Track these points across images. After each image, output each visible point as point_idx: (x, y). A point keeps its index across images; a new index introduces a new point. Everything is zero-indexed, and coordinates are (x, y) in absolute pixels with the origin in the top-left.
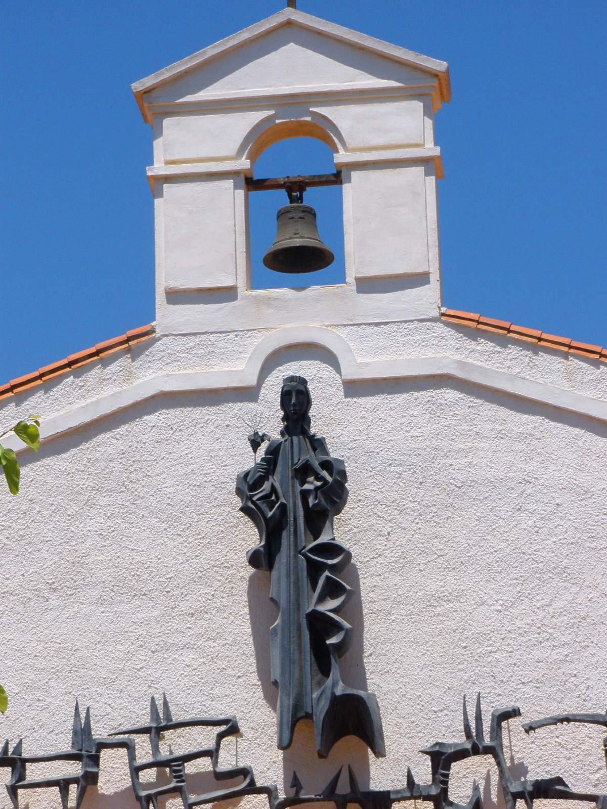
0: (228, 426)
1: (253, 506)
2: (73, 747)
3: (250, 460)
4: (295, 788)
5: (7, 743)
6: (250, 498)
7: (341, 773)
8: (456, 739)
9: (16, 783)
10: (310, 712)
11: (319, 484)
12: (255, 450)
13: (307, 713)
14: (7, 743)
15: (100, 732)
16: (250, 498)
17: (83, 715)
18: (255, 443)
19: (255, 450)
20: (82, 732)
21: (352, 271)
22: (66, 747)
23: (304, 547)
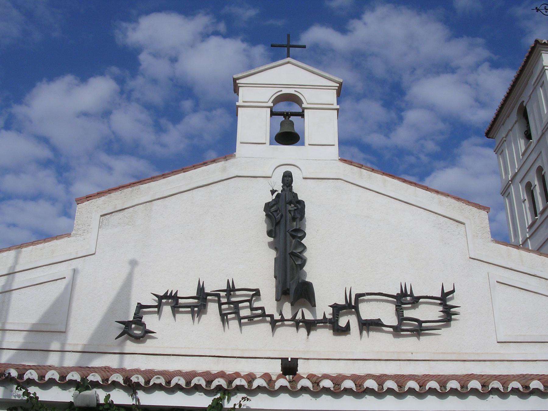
0: (260, 189)
1: (271, 214)
2: (197, 295)
3: (270, 198)
4: (281, 316)
5: (168, 291)
6: (270, 211)
7: (435, 336)
8: (342, 302)
9: (175, 305)
10: (289, 288)
11: (296, 208)
12: (272, 195)
13: (288, 288)
14: (168, 291)
15: (207, 290)
16: (270, 211)
17: (201, 284)
18: (273, 192)
19: (272, 195)
20: (201, 289)
21: (307, 143)
22: (194, 294)
23: (289, 230)
